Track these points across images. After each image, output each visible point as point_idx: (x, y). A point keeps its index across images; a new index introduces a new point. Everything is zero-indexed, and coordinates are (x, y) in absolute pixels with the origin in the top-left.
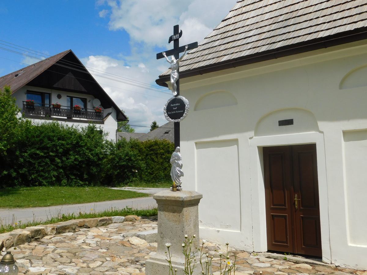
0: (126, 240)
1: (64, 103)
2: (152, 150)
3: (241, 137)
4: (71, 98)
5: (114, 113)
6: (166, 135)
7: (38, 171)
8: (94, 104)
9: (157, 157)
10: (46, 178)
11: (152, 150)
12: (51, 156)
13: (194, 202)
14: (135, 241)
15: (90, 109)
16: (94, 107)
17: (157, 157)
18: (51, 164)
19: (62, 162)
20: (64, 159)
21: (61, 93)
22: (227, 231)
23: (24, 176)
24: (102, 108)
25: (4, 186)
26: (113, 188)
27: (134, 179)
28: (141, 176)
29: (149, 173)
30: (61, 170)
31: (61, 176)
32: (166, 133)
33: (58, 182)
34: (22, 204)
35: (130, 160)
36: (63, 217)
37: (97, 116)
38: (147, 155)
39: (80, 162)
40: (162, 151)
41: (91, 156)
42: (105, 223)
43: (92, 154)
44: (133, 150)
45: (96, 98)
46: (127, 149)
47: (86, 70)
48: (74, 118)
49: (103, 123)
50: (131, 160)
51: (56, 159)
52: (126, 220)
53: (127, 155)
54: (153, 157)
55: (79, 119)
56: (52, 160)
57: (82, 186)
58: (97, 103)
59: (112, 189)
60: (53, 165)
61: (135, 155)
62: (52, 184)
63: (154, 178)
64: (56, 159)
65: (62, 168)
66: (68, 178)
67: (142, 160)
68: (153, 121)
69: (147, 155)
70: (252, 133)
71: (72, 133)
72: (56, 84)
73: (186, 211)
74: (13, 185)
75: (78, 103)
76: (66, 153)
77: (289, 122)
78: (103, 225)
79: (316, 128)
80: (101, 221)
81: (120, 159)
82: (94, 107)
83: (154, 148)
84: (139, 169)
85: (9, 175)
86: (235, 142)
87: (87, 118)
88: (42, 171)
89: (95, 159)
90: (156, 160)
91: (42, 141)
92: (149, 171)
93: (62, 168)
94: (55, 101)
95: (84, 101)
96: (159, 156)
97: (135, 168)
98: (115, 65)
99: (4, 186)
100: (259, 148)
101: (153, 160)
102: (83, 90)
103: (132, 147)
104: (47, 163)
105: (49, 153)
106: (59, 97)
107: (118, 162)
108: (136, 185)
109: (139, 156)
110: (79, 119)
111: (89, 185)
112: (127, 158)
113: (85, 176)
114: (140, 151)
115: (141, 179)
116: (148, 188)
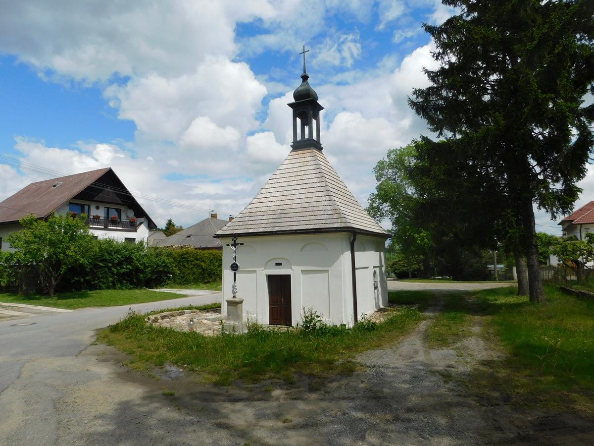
0: (200, 321)
1: (101, 213)
2: (184, 258)
3: (259, 270)
4: (108, 209)
5: (146, 223)
6: (188, 238)
7: (99, 278)
8: (128, 215)
9: (188, 264)
10: (104, 283)
11: (184, 258)
12: (109, 266)
13: (241, 302)
14: (205, 321)
15: (124, 218)
16: (127, 217)
17: (188, 264)
18: (108, 272)
19: (118, 270)
20: (119, 268)
21: (99, 204)
22: (323, 267)
23: (88, 282)
24: (135, 218)
25: (73, 290)
26: (150, 290)
27: (169, 282)
28: (174, 280)
29: (181, 277)
30: (116, 277)
31: (115, 281)
32: (188, 237)
33: (114, 287)
34: (106, 304)
35: (166, 266)
36: (161, 311)
37: (131, 225)
38: (179, 262)
39: (130, 270)
40: (192, 259)
41: (140, 266)
42: (182, 314)
43: (140, 264)
44: (168, 259)
45: (130, 209)
46: (164, 258)
47: (130, 194)
48: (109, 228)
49: (136, 231)
50: (167, 267)
51: (112, 268)
52: (192, 312)
53: (164, 262)
54: (185, 264)
55: (115, 228)
56: (110, 269)
57: (131, 289)
58: (131, 214)
59: (156, 292)
60: (110, 272)
61: (170, 263)
62: (108, 288)
63: (185, 281)
64: (112, 268)
65: (117, 275)
66: (121, 283)
67: (176, 267)
68: (169, 218)
69: (179, 262)
70: (263, 268)
71: (109, 242)
72: (96, 197)
73: (239, 305)
74: (79, 289)
75: (113, 214)
76: (120, 264)
77: (280, 264)
78: (181, 315)
79: (291, 268)
80: (180, 312)
81: (158, 265)
82: (127, 217)
83: (186, 256)
84: (173, 274)
85: (79, 281)
86: (255, 271)
87: (122, 227)
88: (102, 278)
89: (142, 267)
90: (187, 266)
91: (103, 256)
92: (181, 275)
93: (117, 275)
94: (94, 212)
95: (119, 212)
96: (189, 263)
97: (170, 273)
98: (122, 156)
99: (73, 290)
100: (266, 275)
101: (184, 266)
102: (120, 202)
103: (167, 256)
104: (106, 272)
105: (107, 264)
106: (97, 208)
107: (156, 268)
108: (172, 287)
109: (173, 263)
110: (115, 228)
111: (137, 288)
112: (164, 264)
113: (135, 281)
114: (174, 259)
115: (175, 282)
116: (182, 290)
